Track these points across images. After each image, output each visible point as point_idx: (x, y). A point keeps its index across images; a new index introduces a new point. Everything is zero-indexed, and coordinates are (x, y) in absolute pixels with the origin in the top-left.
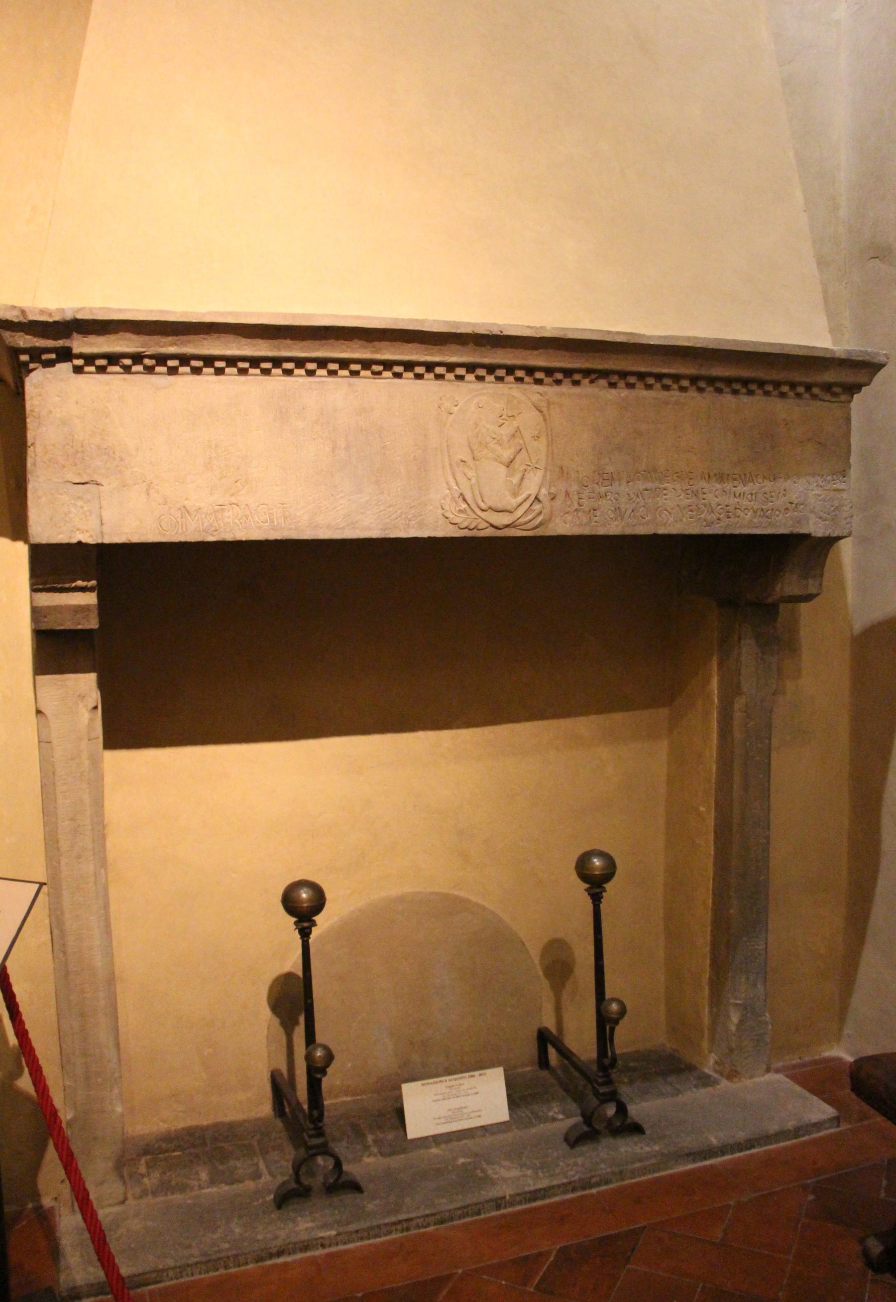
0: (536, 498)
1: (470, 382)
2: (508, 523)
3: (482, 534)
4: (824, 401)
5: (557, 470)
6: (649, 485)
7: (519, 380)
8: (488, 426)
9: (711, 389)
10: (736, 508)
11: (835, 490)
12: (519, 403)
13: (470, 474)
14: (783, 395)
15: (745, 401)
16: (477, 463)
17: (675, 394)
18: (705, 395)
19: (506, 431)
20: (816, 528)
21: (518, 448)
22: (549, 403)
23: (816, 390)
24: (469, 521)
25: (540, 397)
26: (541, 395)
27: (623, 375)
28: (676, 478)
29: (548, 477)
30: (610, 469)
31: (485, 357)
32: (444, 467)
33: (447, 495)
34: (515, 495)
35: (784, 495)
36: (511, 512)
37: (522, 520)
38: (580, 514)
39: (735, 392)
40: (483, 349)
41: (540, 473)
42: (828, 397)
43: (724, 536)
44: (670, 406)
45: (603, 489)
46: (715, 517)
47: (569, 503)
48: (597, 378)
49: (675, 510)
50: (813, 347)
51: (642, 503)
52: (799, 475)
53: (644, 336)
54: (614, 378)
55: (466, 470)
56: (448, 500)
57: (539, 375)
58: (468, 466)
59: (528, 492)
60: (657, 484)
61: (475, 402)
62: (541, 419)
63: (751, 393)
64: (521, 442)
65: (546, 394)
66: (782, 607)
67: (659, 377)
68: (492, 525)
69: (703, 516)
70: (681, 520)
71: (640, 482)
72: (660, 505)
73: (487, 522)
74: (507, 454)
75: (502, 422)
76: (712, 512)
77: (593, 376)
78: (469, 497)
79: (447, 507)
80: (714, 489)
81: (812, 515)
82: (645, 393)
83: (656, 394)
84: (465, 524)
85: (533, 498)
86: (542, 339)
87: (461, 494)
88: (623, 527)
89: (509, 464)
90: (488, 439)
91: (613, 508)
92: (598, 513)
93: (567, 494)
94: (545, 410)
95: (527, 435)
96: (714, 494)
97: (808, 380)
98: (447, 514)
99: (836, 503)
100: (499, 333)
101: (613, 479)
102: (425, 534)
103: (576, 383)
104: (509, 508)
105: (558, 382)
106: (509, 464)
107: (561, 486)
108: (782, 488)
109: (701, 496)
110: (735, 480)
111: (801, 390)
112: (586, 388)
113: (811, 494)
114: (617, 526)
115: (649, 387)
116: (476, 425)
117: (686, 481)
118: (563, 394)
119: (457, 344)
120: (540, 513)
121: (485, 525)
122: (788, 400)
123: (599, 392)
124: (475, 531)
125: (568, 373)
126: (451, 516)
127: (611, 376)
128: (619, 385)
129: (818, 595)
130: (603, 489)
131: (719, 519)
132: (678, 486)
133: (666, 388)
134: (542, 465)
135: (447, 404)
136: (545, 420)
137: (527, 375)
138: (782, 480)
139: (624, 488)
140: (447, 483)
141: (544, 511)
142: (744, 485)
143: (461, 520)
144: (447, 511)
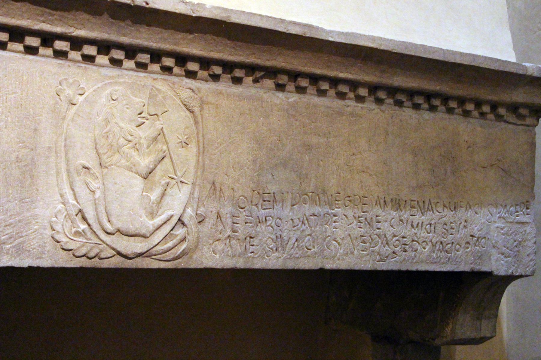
0: (179, 220)
1: (102, 66)
2: (139, 251)
3: (105, 264)
4: (510, 123)
5: (209, 186)
6: (317, 210)
7: (167, 70)
8: (122, 125)
9: (391, 101)
10: (413, 241)
11: (518, 223)
12: (164, 98)
13: (94, 185)
14: (466, 114)
15: (427, 118)
16: (105, 171)
17: (351, 104)
18: (383, 107)
19: (145, 133)
20: (498, 266)
21: (161, 155)
22: (203, 103)
23: (502, 111)
24: (89, 246)
25: (192, 94)
26: (193, 91)
27: (294, 76)
28: (348, 203)
29: (196, 195)
30: (272, 188)
31: (124, 35)
32: (58, 173)
33: (60, 211)
34: (152, 215)
35: (465, 227)
36: (145, 237)
37: (159, 248)
38: (233, 242)
39: (416, 107)
40: (123, 24)
41: (186, 189)
42: (512, 119)
43: (399, 273)
44: (344, 118)
45: (263, 213)
46: (391, 251)
47: (220, 228)
48: (262, 77)
49: (346, 240)
50: (506, 61)
51: (308, 231)
52: (481, 205)
53: (323, 30)
54: (283, 79)
55: (89, 180)
56: (61, 217)
57: (193, 66)
58: (93, 174)
59: (170, 213)
60: (327, 209)
61: (108, 92)
62: (192, 121)
63: (433, 109)
64: (165, 148)
65: (199, 90)
66: (443, 348)
67: (335, 82)
68: (119, 254)
69: (376, 248)
70: (352, 253)
71: (307, 206)
72: (328, 234)
73: (114, 249)
74: (145, 162)
75: (140, 120)
76: (387, 244)
77: (259, 74)
78: (90, 215)
79: (58, 228)
80: (390, 217)
81: (493, 251)
82: (317, 100)
83: (329, 102)
84: (83, 251)
85: (175, 220)
86: (200, 20)
87: (80, 211)
88: (285, 259)
89: (147, 175)
90: (122, 141)
91: (273, 237)
92: (255, 242)
93: (219, 216)
94: (196, 110)
95: (173, 141)
96: (389, 221)
97: (495, 98)
98: (57, 237)
99: (519, 238)
100: (144, 4)
101: (275, 201)
102: (26, 263)
103: (237, 81)
104: (143, 231)
105: (215, 78)
106: (147, 175)
107: (211, 208)
108: (464, 218)
109: (375, 224)
110: (413, 207)
111: (486, 109)
112: (249, 89)
113: (493, 226)
114: (278, 258)
115: (322, 93)
116: (107, 121)
117: (360, 206)
118: (221, 93)
119: (86, 12)
120: (183, 240)
121: (111, 252)
122: (472, 120)
123: (264, 93)
124: (97, 259)
125: (228, 67)
126: (64, 239)
127: (321, 83)
128: (288, 88)
129: (491, 337)
130: (263, 213)
131: (394, 252)
132: (350, 213)
133: (341, 96)
134: (189, 179)
135: (69, 92)
136: (196, 122)
137: (177, 64)
138: (463, 209)
139: (287, 213)
140: (62, 196)
141: (188, 237)
142: (423, 214)
143: (78, 245)
144: (58, 232)
